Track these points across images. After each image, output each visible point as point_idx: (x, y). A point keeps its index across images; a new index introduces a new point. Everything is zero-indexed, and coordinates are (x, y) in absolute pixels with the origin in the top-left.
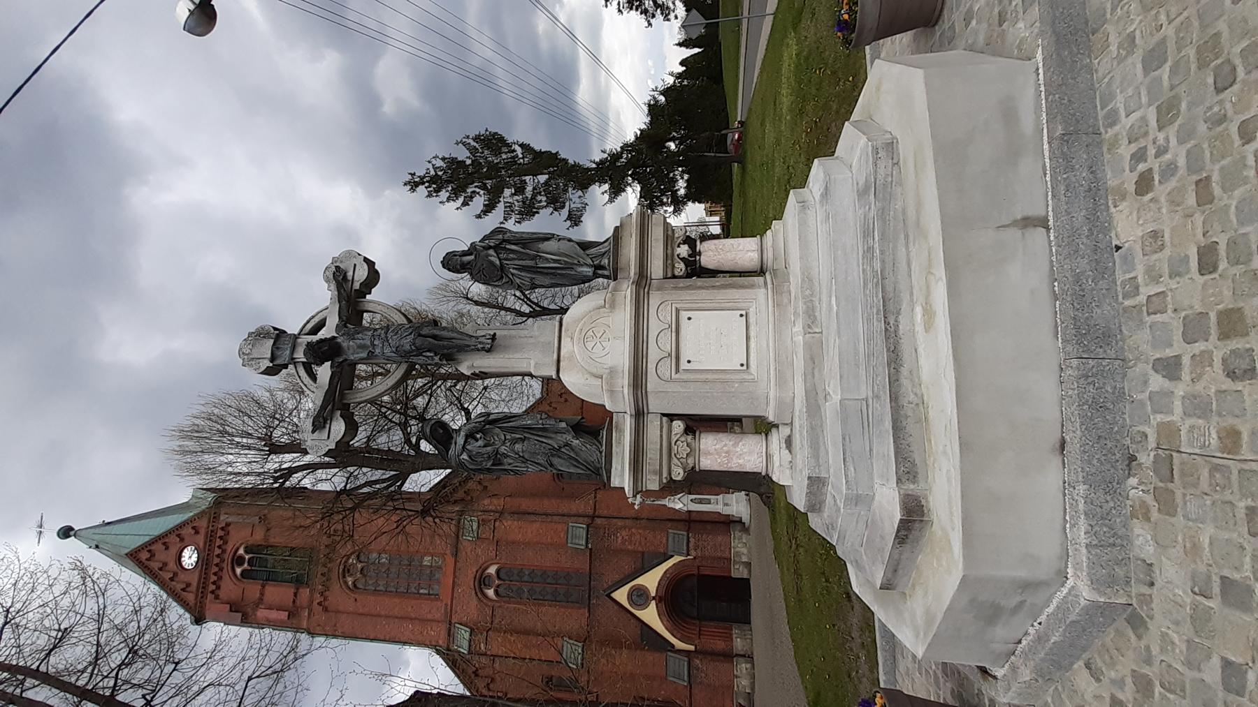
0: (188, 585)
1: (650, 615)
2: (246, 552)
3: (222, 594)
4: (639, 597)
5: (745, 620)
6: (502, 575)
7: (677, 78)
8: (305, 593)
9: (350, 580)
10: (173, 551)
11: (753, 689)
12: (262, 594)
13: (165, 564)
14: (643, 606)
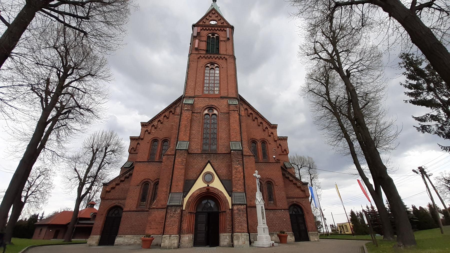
1: (200, 184)
3: (203, 31)
4: (208, 179)
5: (196, 243)
6: (214, 116)
7: (289, 209)
8: (204, 52)
9: (209, 65)
10: (216, 19)
11: (165, 248)
12: (203, 41)
13: (211, 17)
14: (205, 181)
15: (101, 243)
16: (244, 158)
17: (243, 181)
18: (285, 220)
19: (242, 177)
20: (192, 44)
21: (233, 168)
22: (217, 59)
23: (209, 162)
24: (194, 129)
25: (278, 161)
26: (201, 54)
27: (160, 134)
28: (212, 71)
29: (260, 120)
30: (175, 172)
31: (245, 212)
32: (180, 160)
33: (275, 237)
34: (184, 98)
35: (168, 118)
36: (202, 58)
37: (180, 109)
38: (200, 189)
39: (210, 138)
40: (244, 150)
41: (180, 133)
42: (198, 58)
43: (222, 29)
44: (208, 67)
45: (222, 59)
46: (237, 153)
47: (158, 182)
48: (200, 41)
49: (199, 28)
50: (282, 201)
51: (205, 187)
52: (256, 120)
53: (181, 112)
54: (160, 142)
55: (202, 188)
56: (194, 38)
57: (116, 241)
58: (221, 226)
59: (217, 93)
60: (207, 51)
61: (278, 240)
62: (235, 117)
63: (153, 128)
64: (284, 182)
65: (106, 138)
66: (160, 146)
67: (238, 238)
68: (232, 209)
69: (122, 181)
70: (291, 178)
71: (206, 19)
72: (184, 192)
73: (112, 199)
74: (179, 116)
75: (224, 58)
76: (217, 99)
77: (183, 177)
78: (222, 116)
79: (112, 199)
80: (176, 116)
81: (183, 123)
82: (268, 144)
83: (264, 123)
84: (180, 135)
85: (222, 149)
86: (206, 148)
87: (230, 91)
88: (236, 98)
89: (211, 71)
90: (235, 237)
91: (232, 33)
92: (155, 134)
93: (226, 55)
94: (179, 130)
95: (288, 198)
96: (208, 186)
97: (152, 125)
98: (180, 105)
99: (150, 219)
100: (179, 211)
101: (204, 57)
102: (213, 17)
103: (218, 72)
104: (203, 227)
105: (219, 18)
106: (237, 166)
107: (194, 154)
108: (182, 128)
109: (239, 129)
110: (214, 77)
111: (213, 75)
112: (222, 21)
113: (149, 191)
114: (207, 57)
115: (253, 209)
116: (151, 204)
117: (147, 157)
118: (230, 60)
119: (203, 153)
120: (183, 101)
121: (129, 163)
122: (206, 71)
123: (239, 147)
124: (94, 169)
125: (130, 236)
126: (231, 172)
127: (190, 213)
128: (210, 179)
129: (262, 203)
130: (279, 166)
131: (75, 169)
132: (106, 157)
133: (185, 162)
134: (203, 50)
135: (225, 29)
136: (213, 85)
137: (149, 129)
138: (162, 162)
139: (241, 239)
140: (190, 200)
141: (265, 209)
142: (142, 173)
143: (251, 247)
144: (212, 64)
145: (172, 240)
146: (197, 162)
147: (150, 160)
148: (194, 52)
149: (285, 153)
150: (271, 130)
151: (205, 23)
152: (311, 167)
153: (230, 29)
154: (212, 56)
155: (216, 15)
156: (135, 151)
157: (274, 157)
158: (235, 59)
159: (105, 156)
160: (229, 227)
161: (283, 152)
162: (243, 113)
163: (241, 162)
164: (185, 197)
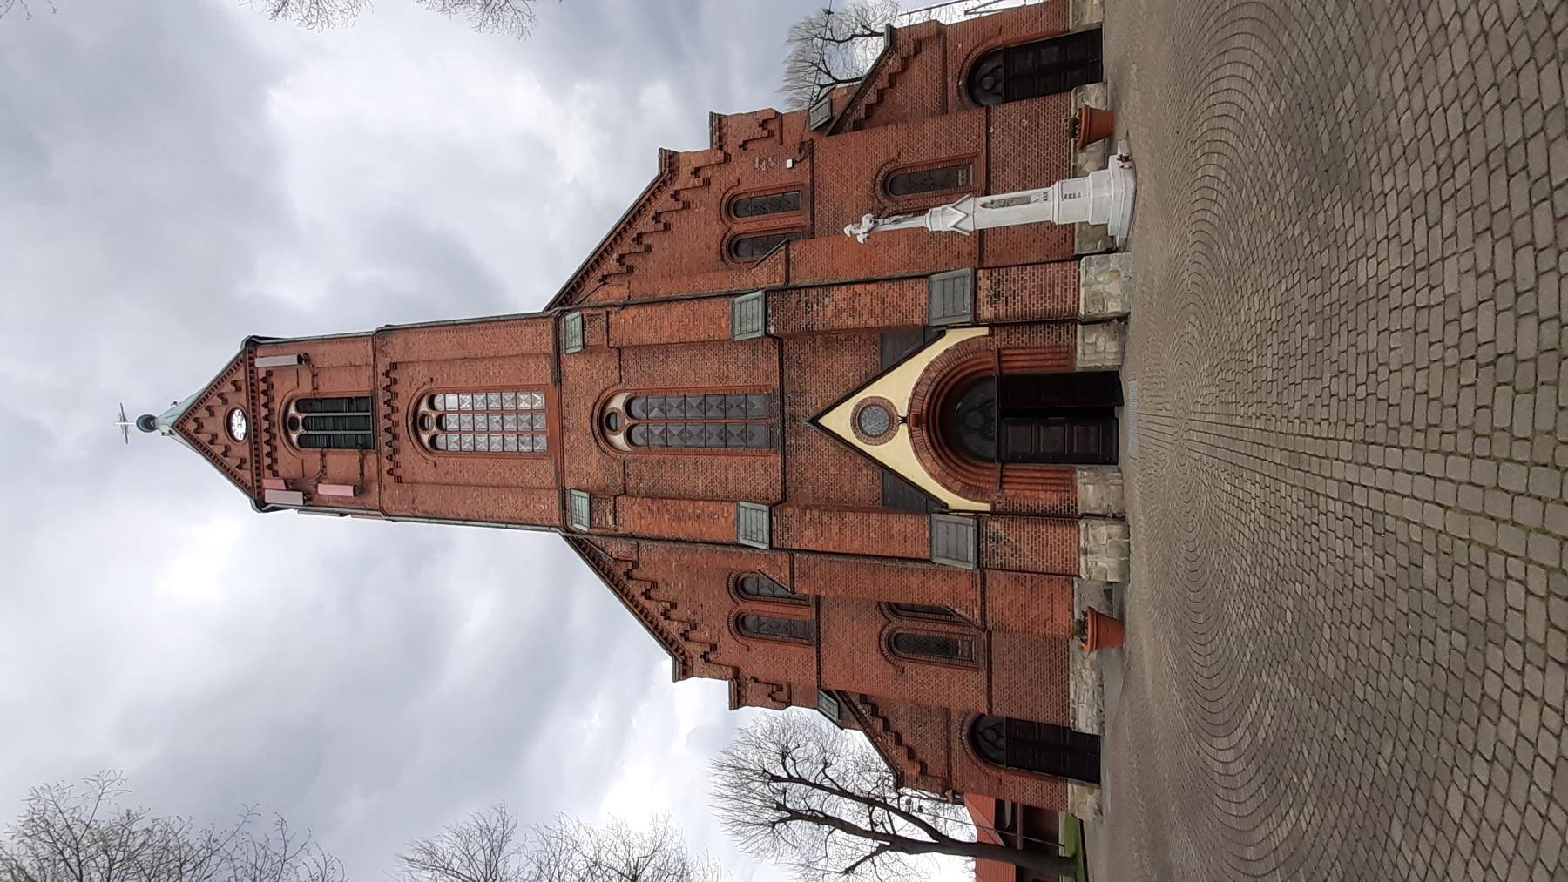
0: (243, 461)
1: (900, 454)
2: (298, 409)
3: (280, 467)
4: (875, 420)
5: (1105, 455)
6: (636, 408)
8: (371, 459)
9: (425, 438)
13: (215, 436)
14: (886, 434)
15: (1091, 776)
16: (798, 282)
17: (887, 285)
18: (1025, 122)
19: (870, 287)
20: (340, 508)
21: (837, 324)
22: (395, 403)
23: (814, 421)
24: (688, 486)
25: (806, 150)
26: (379, 471)
27: (716, 607)
28: (452, 423)
29: (645, 224)
30: (856, 547)
31: (1003, 271)
32: (809, 533)
33: (1086, 159)
34: (567, 530)
35: (654, 584)
36: (397, 465)
37: (613, 541)
38: (915, 451)
39: (720, 421)
40: (765, 283)
41: (707, 537)
42: (399, 480)
43: (263, 386)
44: (433, 440)
45: (395, 381)
46: (776, 309)
47: (889, 605)
48: (323, 476)
49: (266, 483)
50: (959, 132)
51: (910, 431)
52: (646, 240)
53: (625, 536)
54: (745, 606)
55: (914, 445)
56: (311, 503)
57: (1089, 731)
58: (1048, 366)
59: (540, 400)
60: (365, 446)
61: (1096, 147)
62: (632, 325)
63: (692, 635)
64: (887, 124)
65: (742, 785)
66: (758, 607)
67: (1098, 299)
68: (992, 325)
69: (887, 726)
70: (871, 97)
71: (225, 454)
72: (928, 512)
73: (949, 751)
74: (642, 543)
75: (387, 374)
76: (566, 398)
77: (874, 518)
78: (633, 375)
79: (949, 751)
80: (644, 556)
81: (665, 526)
82: (741, 189)
83: (657, 206)
84: (714, 538)
85: (765, 371)
86: (759, 433)
87: (527, 348)
88: (558, 320)
89: (453, 426)
90: (1095, 311)
91: (277, 345)
92: (715, 627)
93: (375, 367)
94: (694, 542)
95: (944, 110)
96: (904, 420)
97: (681, 641)
98: (600, 541)
99: (1018, 625)
100: (996, 526)
101: (390, 458)
102: (214, 425)
103: (452, 400)
104: (1053, 434)
105: (215, 401)
106: (829, 310)
107: (784, 482)
108: (690, 529)
109: (680, 307)
110: (473, 412)
111: (467, 418)
112: (228, 388)
113: (920, 635)
114: (389, 444)
115: (989, 245)
116: (966, 623)
117: (801, 650)
118: (396, 349)
119: (780, 443)
120: (581, 532)
121: (824, 703)
122: (454, 447)
123: (751, 307)
124: (847, 810)
125: (1072, 683)
126: (857, 331)
127: (1001, 483)
128: (882, 418)
129: (971, 204)
130: (824, 144)
131: (848, 871)
132: (805, 776)
133: (816, 513)
134: (362, 462)
135: (262, 375)
136: (509, 418)
137: (700, 650)
138: (818, 597)
139: (1102, 285)
140: (958, 486)
141: (987, 193)
142: (855, 654)
143: (1133, 246)
144: (419, 423)
145: (1098, 544)
146: (814, 463)
147: (812, 636)
148: (373, 499)
149: (773, 126)
150: (684, 179)
151: (243, 461)
152: (827, 31)
153: (260, 352)
154: (384, 424)
155: (202, 413)
156: (780, 689)
157: (789, 164)
158: (386, 332)
159: (800, 780)
160: (1053, 338)
161: (771, 134)
162: (616, 292)
163: (814, 292)
164: (946, 506)
